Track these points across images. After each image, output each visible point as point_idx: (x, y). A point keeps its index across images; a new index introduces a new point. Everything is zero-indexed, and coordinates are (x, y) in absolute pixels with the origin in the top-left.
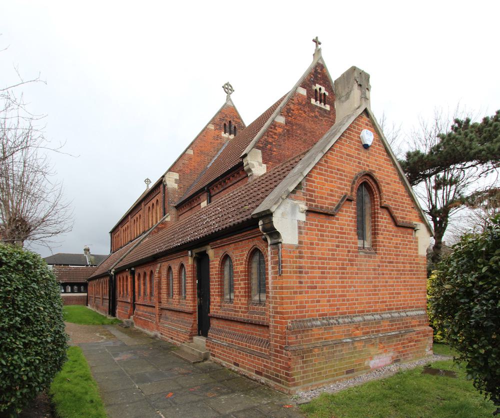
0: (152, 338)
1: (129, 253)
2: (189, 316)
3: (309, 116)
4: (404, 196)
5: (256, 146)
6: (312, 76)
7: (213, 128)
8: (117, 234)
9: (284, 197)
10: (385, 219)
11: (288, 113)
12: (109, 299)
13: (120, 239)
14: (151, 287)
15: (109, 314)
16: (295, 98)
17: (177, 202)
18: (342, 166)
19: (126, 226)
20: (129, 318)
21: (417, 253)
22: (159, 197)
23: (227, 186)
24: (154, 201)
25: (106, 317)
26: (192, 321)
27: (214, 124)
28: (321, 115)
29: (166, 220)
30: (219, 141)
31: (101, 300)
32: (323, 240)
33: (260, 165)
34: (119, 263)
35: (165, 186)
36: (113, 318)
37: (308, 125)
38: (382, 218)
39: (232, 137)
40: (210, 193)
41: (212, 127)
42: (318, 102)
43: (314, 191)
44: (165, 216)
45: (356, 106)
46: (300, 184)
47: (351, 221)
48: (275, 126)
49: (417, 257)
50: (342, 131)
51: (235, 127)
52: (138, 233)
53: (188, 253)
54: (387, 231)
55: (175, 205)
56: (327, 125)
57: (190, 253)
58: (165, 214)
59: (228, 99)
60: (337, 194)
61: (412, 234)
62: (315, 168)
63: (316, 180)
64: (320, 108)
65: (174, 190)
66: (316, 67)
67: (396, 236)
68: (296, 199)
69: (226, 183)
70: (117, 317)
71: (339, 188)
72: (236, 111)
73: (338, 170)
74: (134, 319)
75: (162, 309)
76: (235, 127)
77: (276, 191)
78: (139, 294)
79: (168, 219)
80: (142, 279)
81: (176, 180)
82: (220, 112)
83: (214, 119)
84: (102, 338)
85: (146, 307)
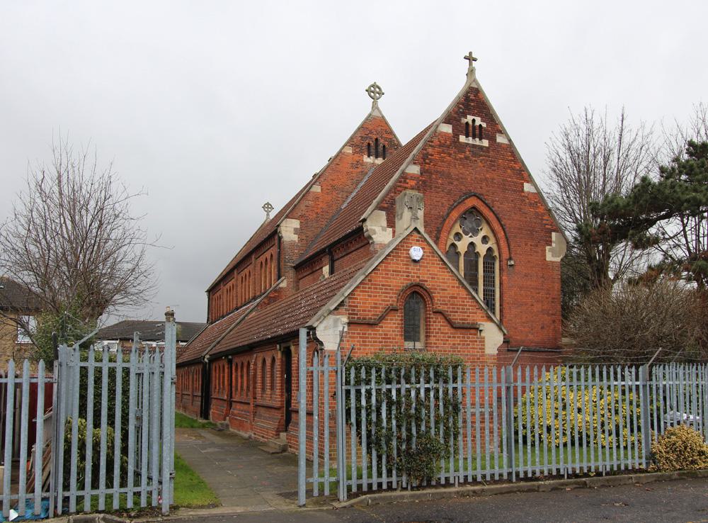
0: (246, 439)
1: (229, 333)
2: (277, 411)
3: (455, 159)
4: (466, 298)
5: (380, 207)
6: (461, 106)
7: (351, 152)
8: (218, 294)
9: (326, 315)
10: (439, 322)
11: (424, 160)
12: (202, 396)
13: (221, 303)
14: (248, 380)
15: (201, 416)
16: (436, 140)
17: (297, 260)
18: (388, 282)
19: (230, 284)
20: (225, 420)
21: (484, 352)
22: (274, 250)
23: (349, 251)
24: (267, 255)
25: (196, 420)
26: (278, 416)
27: (352, 145)
28: (474, 155)
29: (281, 285)
30: (359, 170)
31: (190, 397)
32: (365, 345)
33: (384, 229)
34: (215, 346)
35: (280, 238)
36: (205, 421)
37: (454, 171)
38: (435, 322)
39: (379, 161)
40: (333, 257)
41: (349, 150)
42: (470, 138)
43: (357, 307)
44: (280, 281)
45: (406, 227)
46: (343, 302)
47: (396, 328)
48: (406, 178)
49: (483, 356)
50: (387, 253)
51: (384, 146)
52: (247, 297)
53: (276, 347)
54: (442, 333)
55: (293, 265)
56: (484, 166)
57: (278, 346)
58: (279, 277)
59: (375, 106)
60: (381, 306)
61: (475, 334)
62: (357, 287)
63: (359, 297)
64: (474, 146)
65: (292, 244)
66: (467, 92)
67: (454, 337)
68: (339, 314)
69: (349, 248)
70: (211, 420)
71: (384, 300)
72: (386, 123)
73: (383, 285)
74: (230, 421)
75: (257, 406)
76: (384, 146)
77: (324, 308)
78: (237, 389)
79: (284, 285)
80: (239, 370)
81: (296, 229)
82: (362, 127)
83: (352, 138)
84: (191, 439)
85: (243, 405)
